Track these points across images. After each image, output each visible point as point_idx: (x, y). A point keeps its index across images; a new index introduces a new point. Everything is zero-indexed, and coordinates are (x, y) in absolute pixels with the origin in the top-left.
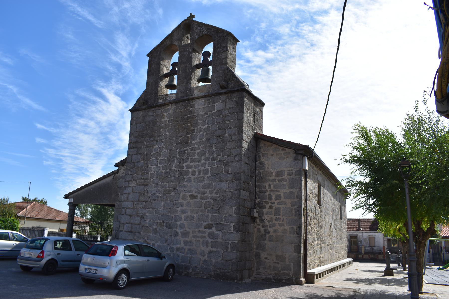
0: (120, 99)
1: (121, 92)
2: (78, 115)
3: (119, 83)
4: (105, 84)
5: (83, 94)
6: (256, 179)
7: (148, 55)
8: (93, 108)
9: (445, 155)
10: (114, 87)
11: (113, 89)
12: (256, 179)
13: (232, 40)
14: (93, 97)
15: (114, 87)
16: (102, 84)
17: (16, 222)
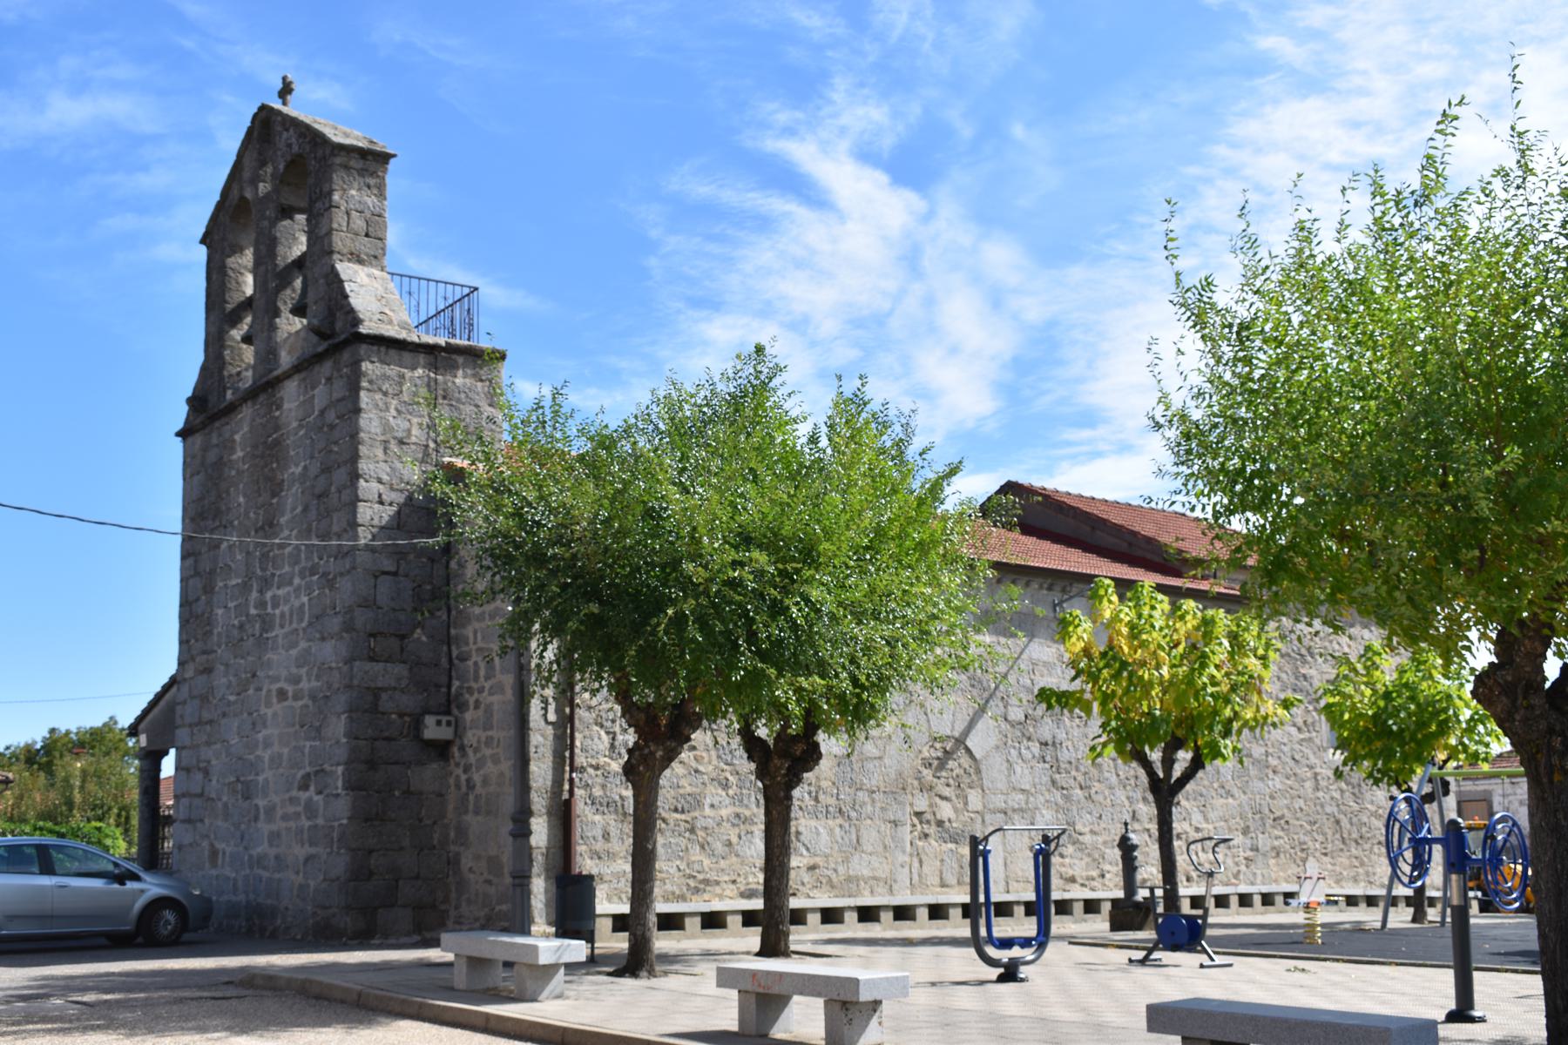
0: (883, 178)
1: (888, 142)
2: (698, 303)
3: (866, 91)
4: (800, 115)
5: (703, 190)
6: (449, 617)
7: (203, 241)
8: (760, 254)
9: (1273, 413)
10: (845, 120)
11: (843, 131)
12: (449, 617)
13: (352, 163)
14: (750, 195)
15: (845, 120)
16: (783, 117)
17: (107, 836)
